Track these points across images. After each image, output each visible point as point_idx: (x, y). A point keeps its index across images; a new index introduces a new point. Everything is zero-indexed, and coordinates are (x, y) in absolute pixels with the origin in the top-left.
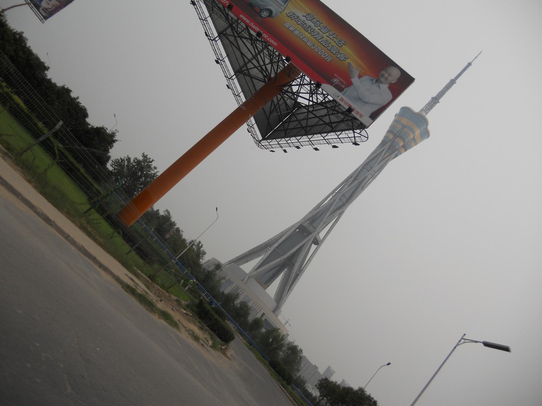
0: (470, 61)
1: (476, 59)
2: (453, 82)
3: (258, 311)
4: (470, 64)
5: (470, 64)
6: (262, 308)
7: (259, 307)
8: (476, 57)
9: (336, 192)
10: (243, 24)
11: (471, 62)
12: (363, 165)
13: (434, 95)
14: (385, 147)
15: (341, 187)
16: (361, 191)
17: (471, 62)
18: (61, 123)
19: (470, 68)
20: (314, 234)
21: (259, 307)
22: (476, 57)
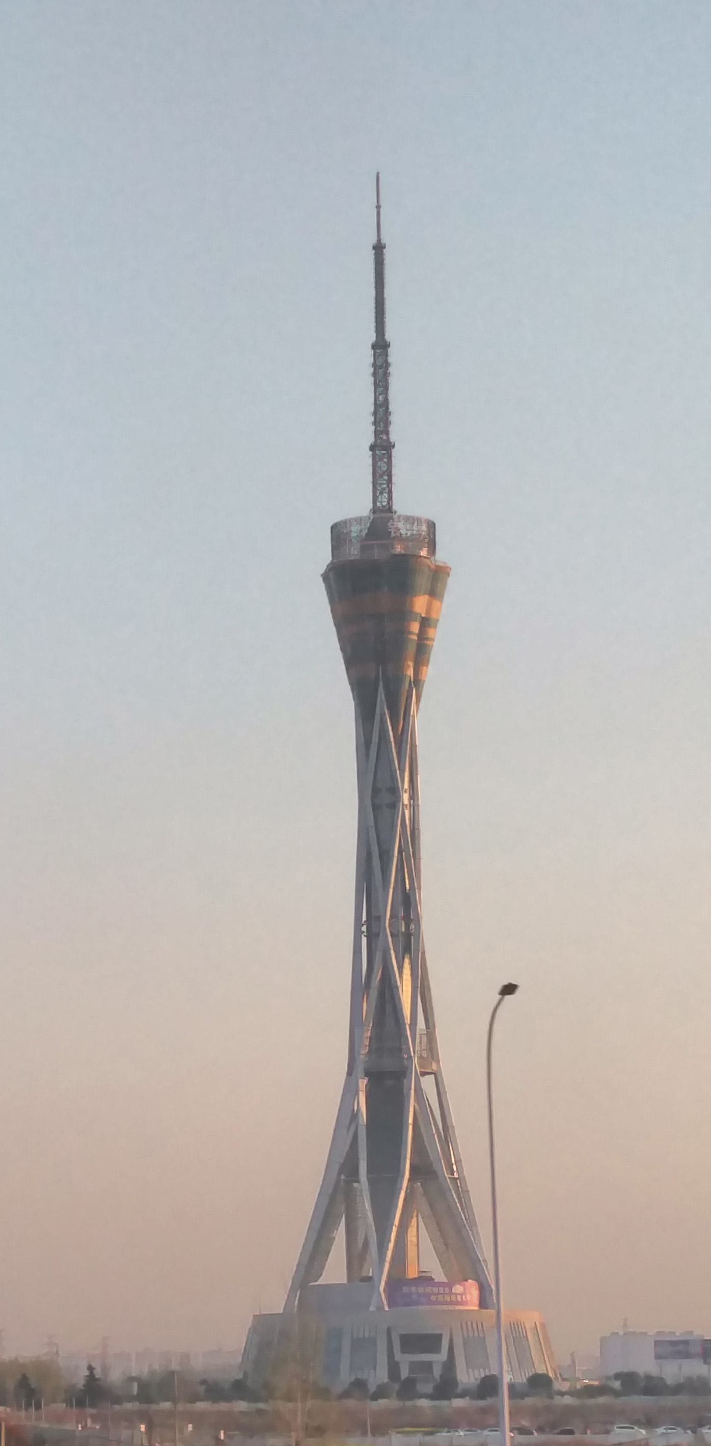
0: (374, 240)
1: (382, 210)
2: (381, 347)
3: (481, 1335)
4: (379, 249)
5: (379, 249)
6: (482, 1323)
7: (469, 1324)
8: (378, 207)
9: (364, 918)
10: (425, 1039)
11: (379, 240)
12: (368, 802)
13: (369, 438)
14: (378, 712)
15: (451, 1148)
16: (417, 860)
17: (379, 240)
18: (222, 1437)
19: (388, 254)
20: (381, 699)
21: (469, 1324)
22: (378, 207)
